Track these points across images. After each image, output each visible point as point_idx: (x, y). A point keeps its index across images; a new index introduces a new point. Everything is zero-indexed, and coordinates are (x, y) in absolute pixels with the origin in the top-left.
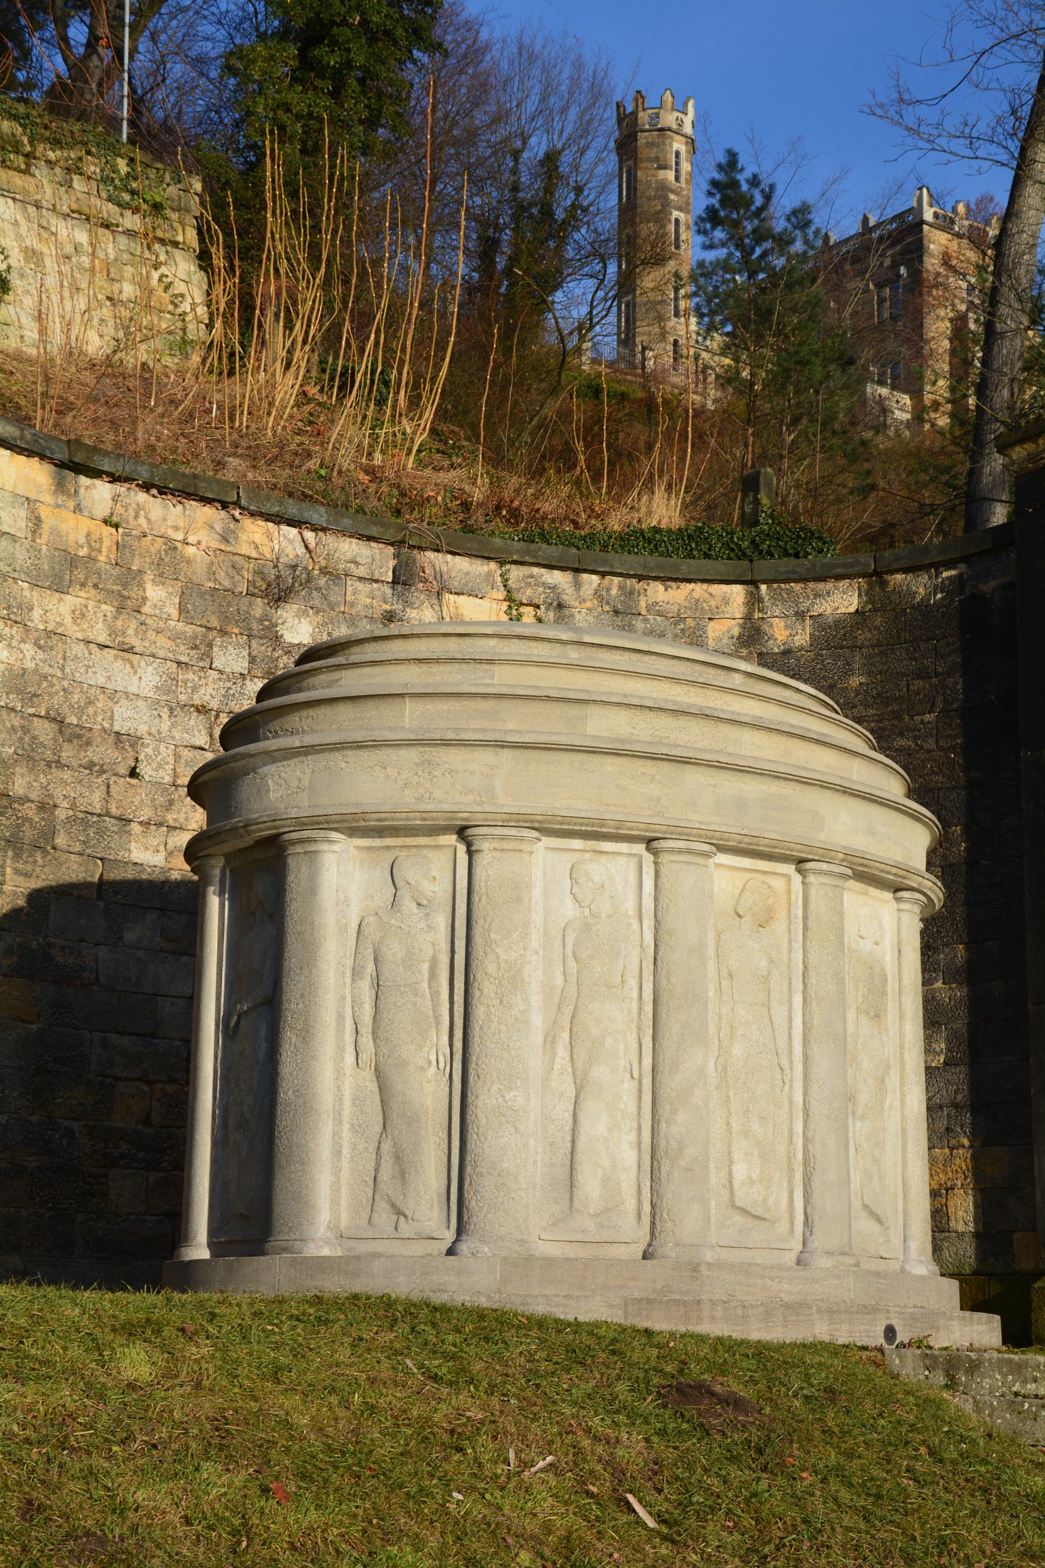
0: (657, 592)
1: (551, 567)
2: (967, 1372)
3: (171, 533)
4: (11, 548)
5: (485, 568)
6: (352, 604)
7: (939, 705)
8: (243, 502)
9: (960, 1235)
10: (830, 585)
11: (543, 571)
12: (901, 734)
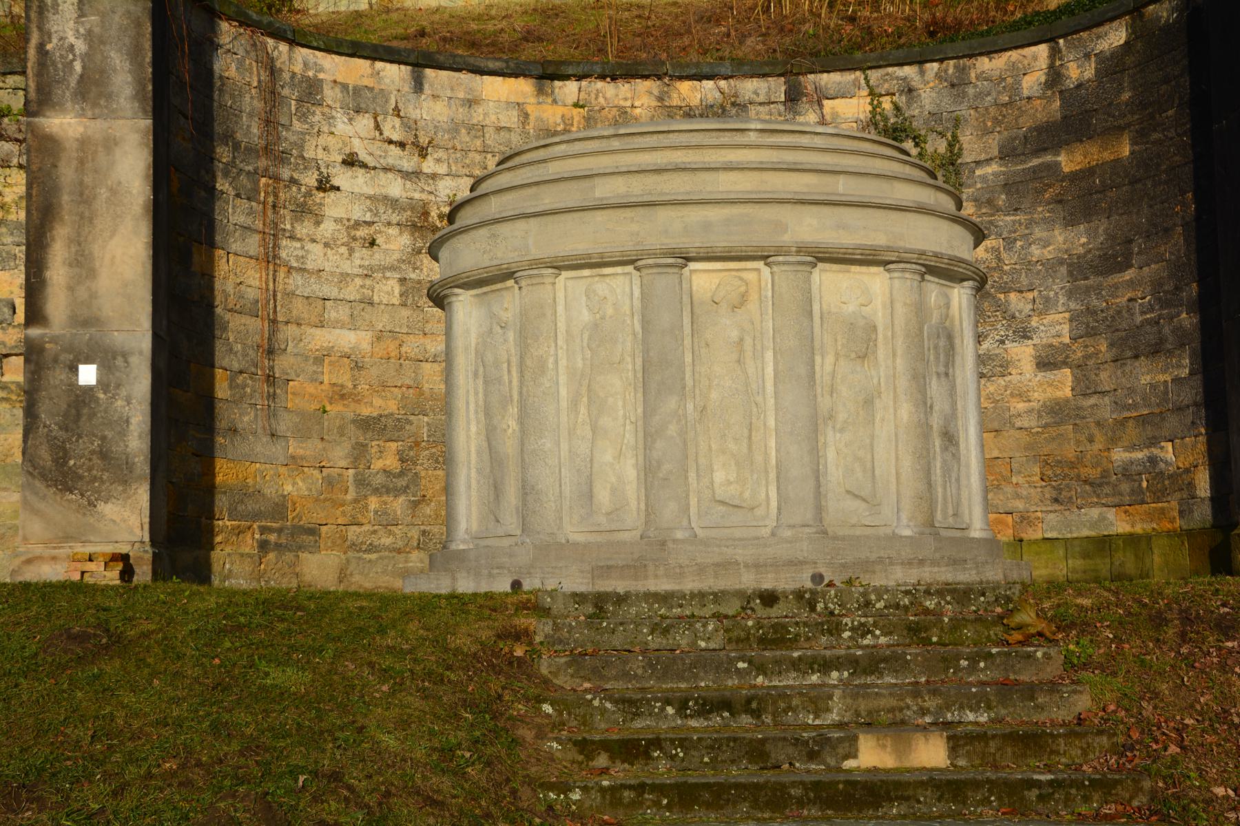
0: (984, 64)
1: (901, 65)
2: (614, 604)
3: (622, 103)
4: (507, 136)
5: (853, 76)
7: (1177, 101)
8: (670, 72)
9: (1203, 499)
10: (1106, 27)
11: (896, 68)
12: (1155, 130)
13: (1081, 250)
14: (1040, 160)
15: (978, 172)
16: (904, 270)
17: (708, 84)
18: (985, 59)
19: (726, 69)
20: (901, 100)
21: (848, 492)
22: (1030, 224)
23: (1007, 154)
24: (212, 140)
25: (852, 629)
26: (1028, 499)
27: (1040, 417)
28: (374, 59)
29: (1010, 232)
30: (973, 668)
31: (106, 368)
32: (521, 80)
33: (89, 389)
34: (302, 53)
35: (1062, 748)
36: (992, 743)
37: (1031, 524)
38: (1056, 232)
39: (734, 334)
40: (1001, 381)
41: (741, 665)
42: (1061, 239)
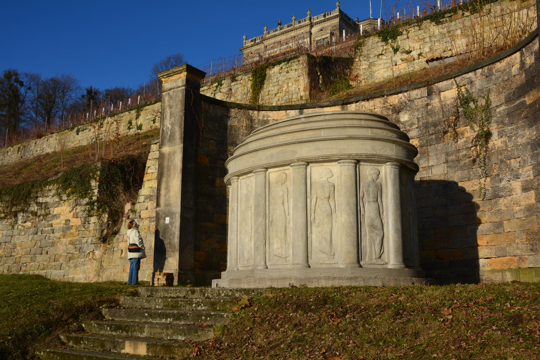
0: (498, 65)
1: (468, 73)
3: (371, 108)
6: (417, 106)
13: (534, 137)
14: (519, 101)
15: (497, 110)
16: (344, 163)
17: (400, 95)
18: (498, 63)
19: (405, 88)
20: (468, 87)
21: (320, 251)
22: (517, 128)
23: (508, 100)
24: (226, 145)
25: (195, 304)
26: (521, 250)
27: (524, 212)
28: (287, 110)
29: (510, 133)
30: (206, 320)
31: (171, 218)
32: (336, 107)
33: (168, 225)
34: (262, 113)
35: (176, 352)
36: (158, 348)
37: (523, 261)
38: (526, 131)
39: (281, 194)
40: (510, 198)
41: (146, 314)
42: (528, 133)
